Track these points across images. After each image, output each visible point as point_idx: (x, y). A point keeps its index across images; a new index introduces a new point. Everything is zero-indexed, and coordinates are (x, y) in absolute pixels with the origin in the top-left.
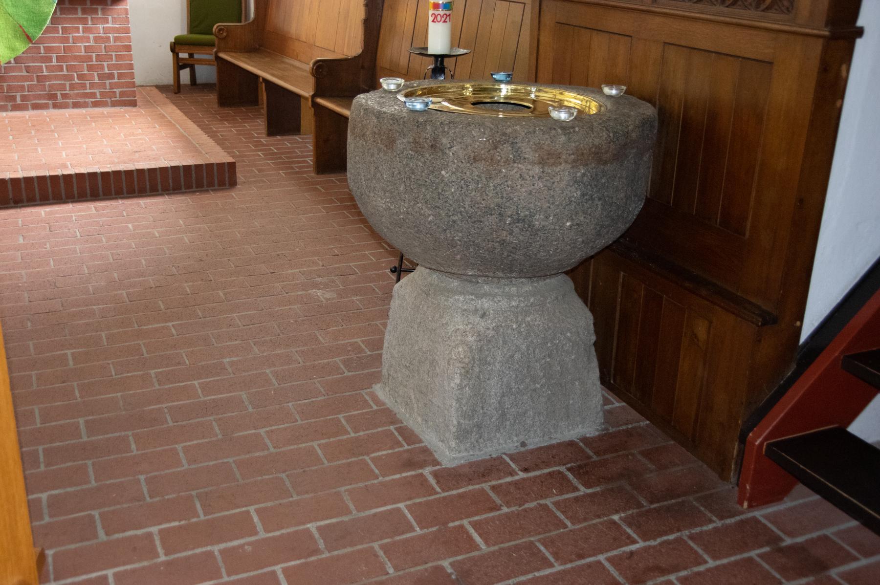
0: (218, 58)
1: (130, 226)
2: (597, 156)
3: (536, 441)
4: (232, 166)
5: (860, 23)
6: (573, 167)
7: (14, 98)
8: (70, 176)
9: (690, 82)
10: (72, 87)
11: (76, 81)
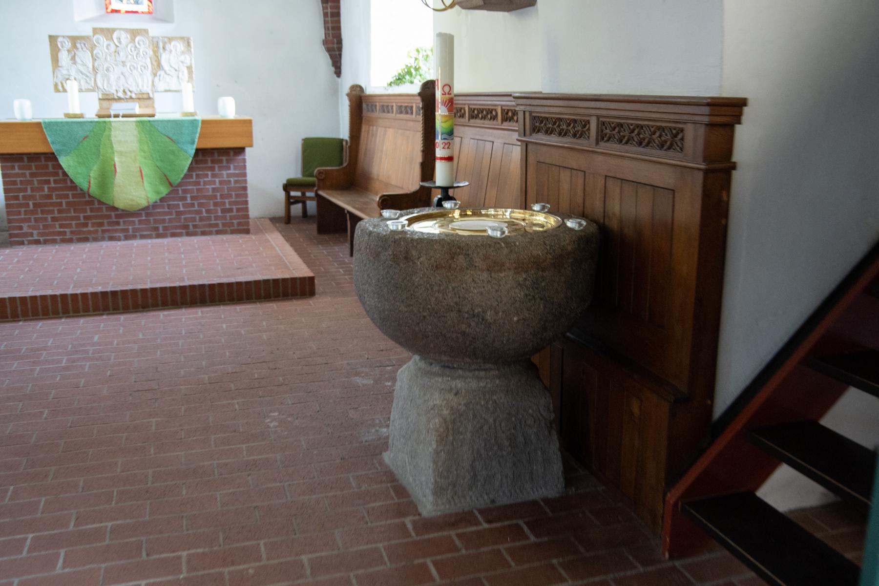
0: (317, 195)
1: (224, 326)
2: (537, 264)
3: (504, 500)
4: (312, 279)
5: (734, 159)
6: (515, 273)
7: (157, 229)
8: (185, 287)
9: (625, 208)
10: (201, 219)
11: (204, 214)
